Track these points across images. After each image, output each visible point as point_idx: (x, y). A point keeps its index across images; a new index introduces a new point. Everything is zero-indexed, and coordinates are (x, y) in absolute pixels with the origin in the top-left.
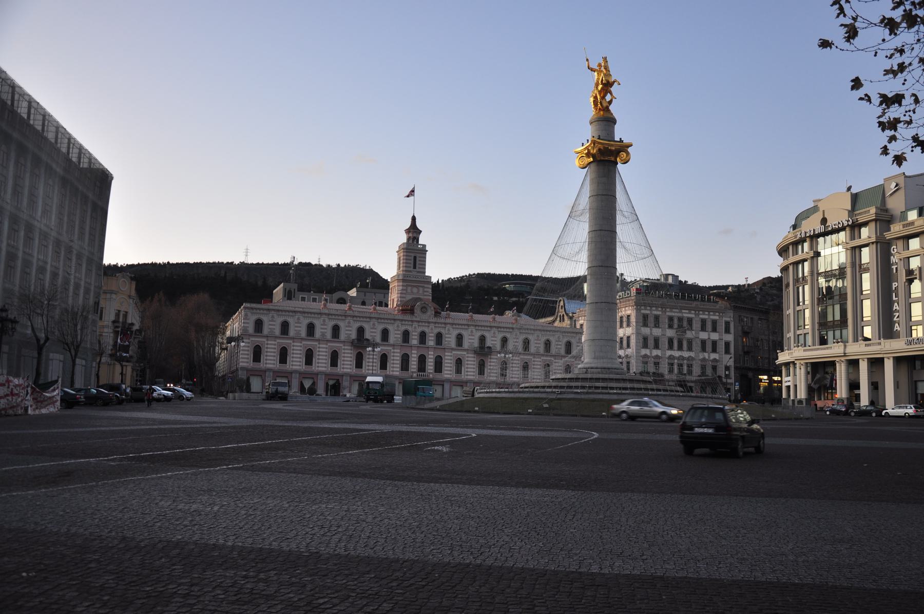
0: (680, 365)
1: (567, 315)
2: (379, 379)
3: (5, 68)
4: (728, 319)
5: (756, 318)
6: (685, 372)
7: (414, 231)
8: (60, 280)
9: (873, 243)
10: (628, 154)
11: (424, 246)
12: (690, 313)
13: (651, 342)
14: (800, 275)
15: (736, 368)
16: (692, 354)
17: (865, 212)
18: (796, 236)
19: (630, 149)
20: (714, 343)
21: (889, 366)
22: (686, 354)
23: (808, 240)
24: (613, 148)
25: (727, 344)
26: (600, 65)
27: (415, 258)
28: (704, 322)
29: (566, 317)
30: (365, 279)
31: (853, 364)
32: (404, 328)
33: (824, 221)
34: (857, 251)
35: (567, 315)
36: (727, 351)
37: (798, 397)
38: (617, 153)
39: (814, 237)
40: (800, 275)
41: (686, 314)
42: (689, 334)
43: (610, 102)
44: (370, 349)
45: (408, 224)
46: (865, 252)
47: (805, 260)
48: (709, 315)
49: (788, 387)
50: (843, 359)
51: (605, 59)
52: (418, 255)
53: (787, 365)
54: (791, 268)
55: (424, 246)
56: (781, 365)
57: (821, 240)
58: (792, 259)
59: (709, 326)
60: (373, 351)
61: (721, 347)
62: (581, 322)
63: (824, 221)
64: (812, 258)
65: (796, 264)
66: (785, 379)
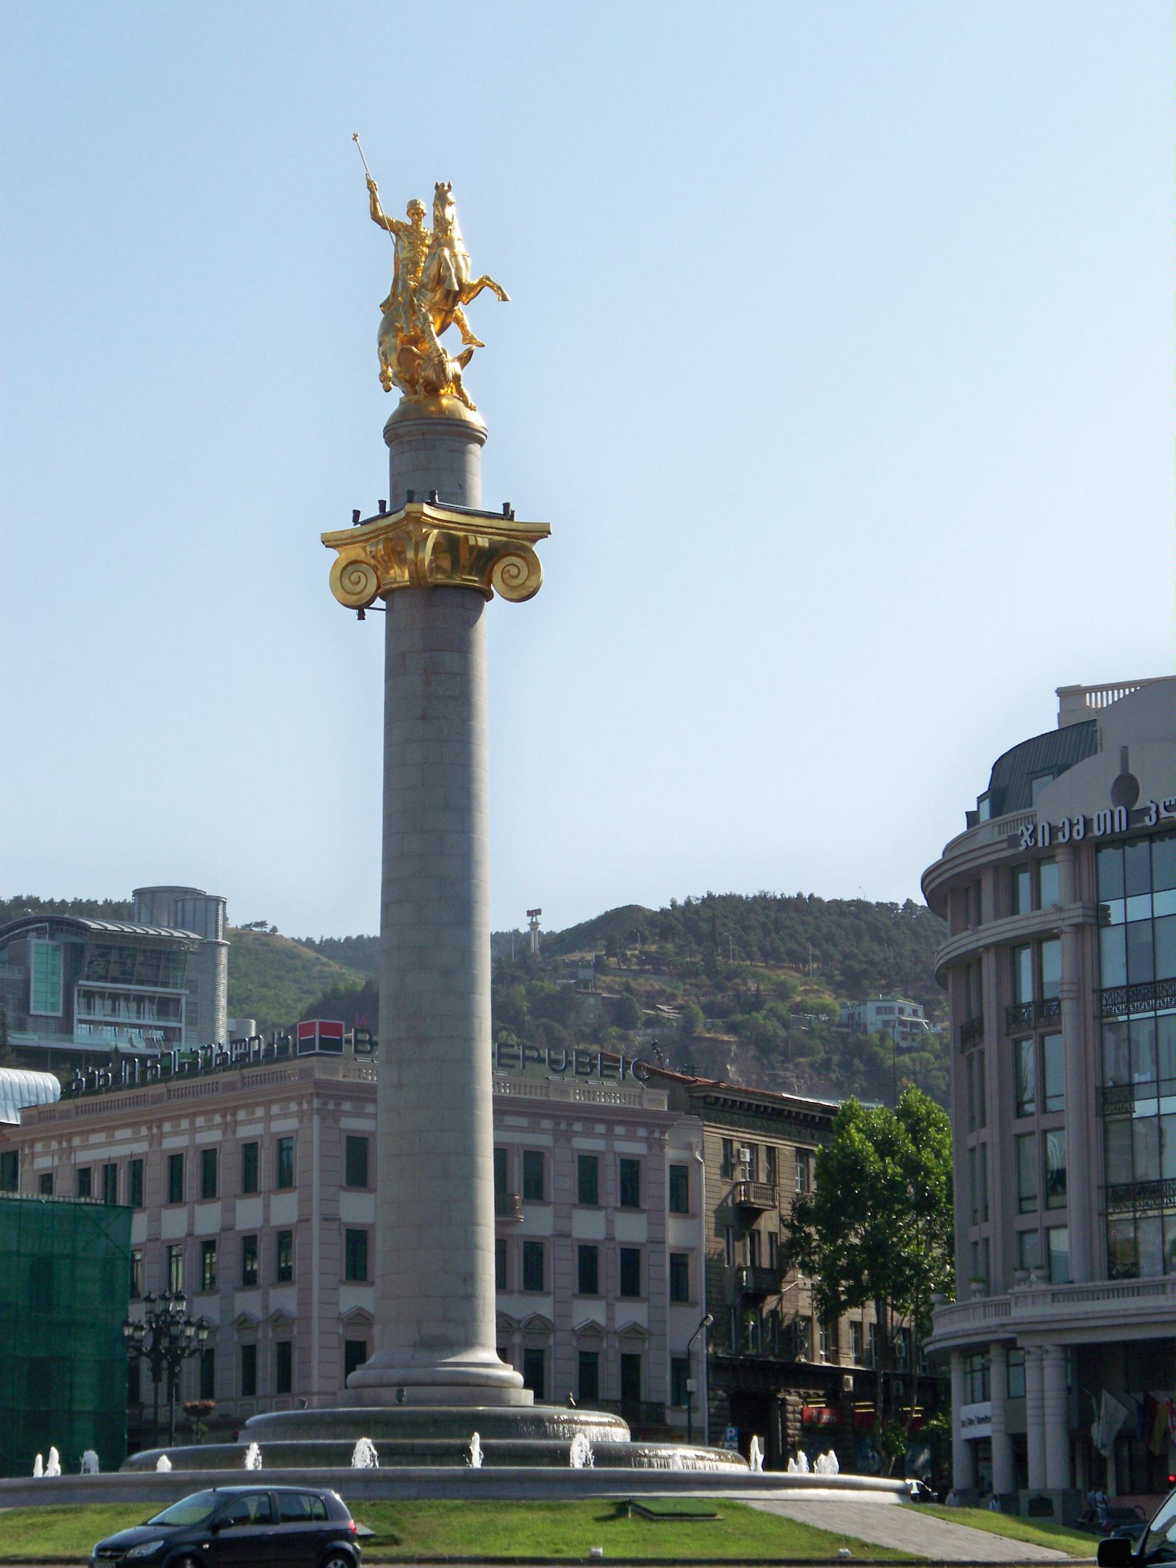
3: (88, 865)
5: (786, 1148)
7: (371, 186)
8: (165, 1375)
10: (533, 565)
12: (534, 1129)
14: (1027, 995)
15: (715, 1365)
18: (1014, 841)
19: (539, 548)
23: (1061, 855)
24: (483, 542)
26: (414, 209)
36: (679, 1292)
38: (485, 560)
39: (1088, 847)
40: (1027, 995)
48: (609, 1136)
49: (979, 1447)
51: (441, 197)
53: (973, 1351)
54: (989, 965)
56: (943, 1356)
57: (1110, 858)
58: (996, 929)
59: (610, 1272)
62: (43, 1163)
63: (1126, 788)
64: (1078, 928)
65: (1010, 948)
66: (962, 1411)
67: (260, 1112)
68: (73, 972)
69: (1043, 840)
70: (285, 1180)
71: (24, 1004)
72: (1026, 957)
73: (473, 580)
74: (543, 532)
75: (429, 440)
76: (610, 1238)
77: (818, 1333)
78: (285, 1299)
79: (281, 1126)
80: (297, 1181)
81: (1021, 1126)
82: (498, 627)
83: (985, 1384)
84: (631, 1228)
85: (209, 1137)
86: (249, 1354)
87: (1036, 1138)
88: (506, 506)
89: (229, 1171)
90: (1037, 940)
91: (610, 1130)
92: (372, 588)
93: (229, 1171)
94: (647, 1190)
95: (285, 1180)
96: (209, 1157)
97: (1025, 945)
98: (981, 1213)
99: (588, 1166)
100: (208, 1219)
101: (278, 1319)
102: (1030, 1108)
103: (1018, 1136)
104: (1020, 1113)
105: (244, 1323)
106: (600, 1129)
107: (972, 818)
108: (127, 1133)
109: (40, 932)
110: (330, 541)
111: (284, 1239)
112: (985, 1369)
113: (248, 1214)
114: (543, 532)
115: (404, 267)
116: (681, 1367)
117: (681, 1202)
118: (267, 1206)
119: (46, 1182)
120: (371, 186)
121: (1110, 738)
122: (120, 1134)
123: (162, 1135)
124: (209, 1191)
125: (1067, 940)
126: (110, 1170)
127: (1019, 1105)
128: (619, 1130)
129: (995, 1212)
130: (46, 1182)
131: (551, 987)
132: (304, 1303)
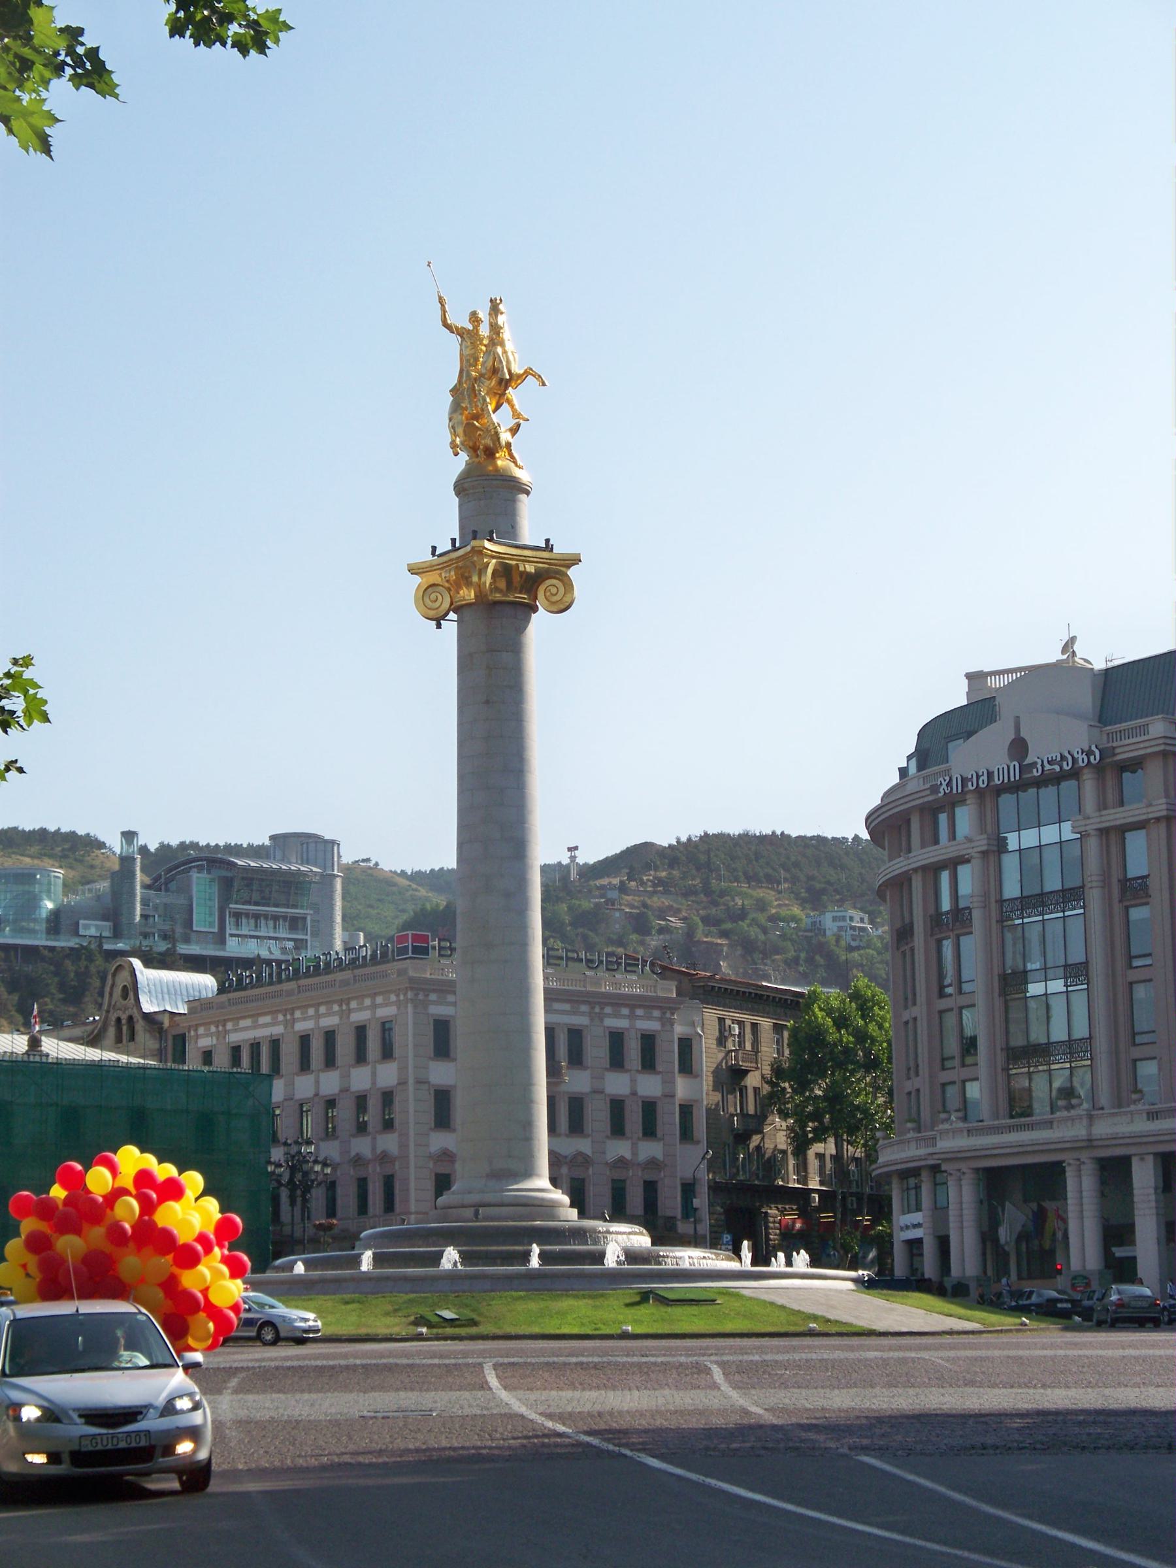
9: (1158, 819)
10: (568, 585)
13: (634, 1119)
14: (946, 905)
15: (715, 1188)
17: (1131, 732)
18: (935, 789)
19: (572, 572)
21: (1144, 1177)
23: (971, 799)
24: (530, 568)
26: (474, 318)
28: (617, 1040)
29: (140, 1025)
31: (1114, 1172)
33: (1019, 747)
34: (1113, 837)
36: (686, 1133)
37: (955, 1271)
38: (532, 583)
39: (990, 793)
40: (946, 905)
46: (1136, 843)
47: (964, 860)
48: (632, 1017)
49: (914, 1245)
50: (1084, 1156)
53: (909, 1174)
54: (917, 882)
58: (922, 856)
59: (634, 1119)
61: (670, 1120)
62: (205, 1043)
63: (1019, 747)
64: (985, 854)
65: (933, 871)
67: (368, 1002)
69: (956, 788)
70: (387, 1053)
71: (189, 923)
72: (945, 876)
73: (524, 597)
74: (575, 560)
75: (488, 491)
76: (634, 1093)
78: (389, 1142)
80: (397, 1052)
81: (944, 1004)
82: (541, 627)
84: (617, 1084)
86: (362, 1183)
87: (956, 1011)
89: (345, 1047)
90: (953, 864)
92: (446, 605)
93: (345, 1047)
95: (387, 1053)
100: (330, 1083)
101: (384, 1158)
104: (942, 995)
105: (358, 1161)
106: (625, 1011)
107: (903, 772)
108: (267, 1019)
109: (200, 869)
110: (414, 570)
111: (387, 1097)
112: (918, 1188)
113: (360, 1079)
114: (575, 560)
115: (467, 361)
116: (688, 1189)
117: (687, 1065)
119: (207, 1057)
121: (1007, 710)
123: (294, 1020)
124: (330, 1061)
125: (976, 863)
126: (255, 1047)
127: (941, 988)
128: (640, 1012)
129: (924, 1070)
130: (207, 1057)
131: (586, 904)
132: (403, 1146)
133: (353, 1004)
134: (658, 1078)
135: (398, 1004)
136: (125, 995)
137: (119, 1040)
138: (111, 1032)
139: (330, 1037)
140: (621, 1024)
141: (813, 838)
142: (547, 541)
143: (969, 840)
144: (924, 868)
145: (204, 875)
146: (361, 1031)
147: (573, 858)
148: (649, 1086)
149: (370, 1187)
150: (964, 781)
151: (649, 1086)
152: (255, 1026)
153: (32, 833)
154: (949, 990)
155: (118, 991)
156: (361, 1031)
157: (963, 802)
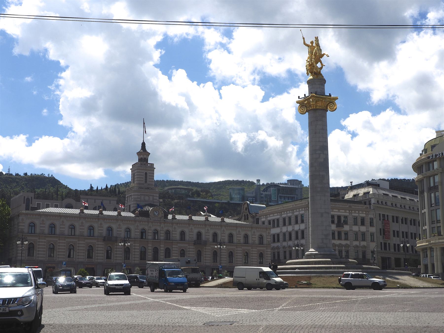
0: (340, 252)
1: (250, 214)
2: (388, 278)
4: (372, 216)
6: (344, 256)
7: (304, 38)
11: (152, 165)
14: (432, 185)
16: (348, 242)
19: (336, 101)
20: (363, 234)
22: (344, 242)
25: (372, 235)
27: (146, 173)
28: (355, 219)
29: (249, 216)
30: (253, 183)
32: (141, 227)
35: (250, 214)
40: (432, 185)
41: (342, 213)
42: (346, 228)
43: (321, 68)
44: (18, 243)
45: (139, 148)
48: (359, 213)
52: (148, 172)
55: (152, 165)
60: (22, 243)
61: (368, 237)
62: (263, 219)
67: (298, 210)
68: (278, 193)
69: (434, 157)
70: (302, 221)
71: (271, 198)
72: (432, 178)
74: (170, 78)
76: (360, 231)
77: (227, 279)
79: (301, 212)
80: (305, 221)
81: (432, 208)
83: (427, 255)
85: (290, 215)
86: (285, 252)
87: (435, 211)
88: (330, 94)
89: (293, 220)
90: (434, 176)
91: (359, 212)
92: (305, 111)
93: (293, 220)
94: (365, 222)
95: (302, 221)
96: (290, 218)
97: (431, 176)
98: (424, 224)
99: (355, 219)
100: (290, 228)
102: (433, 205)
103: (431, 210)
104: (431, 206)
105: (284, 247)
106: (357, 212)
107: (421, 154)
108: (276, 214)
111: (303, 232)
112: (427, 252)
113: (297, 227)
114: (170, 78)
115: (311, 53)
117: (371, 224)
118: (300, 226)
119: (263, 223)
120: (304, 38)
122: (275, 215)
123: (282, 215)
124: (290, 224)
125: (439, 175)
126: (274, 221)
127: (431, 205)
128: (360, 212)
130: (263, 223)
133: (295, 211)
134: (365, 227)
135: (305, 210)
136: (246, 210)
137: (245, 219)
138: (243, 218)
139: (290, 218)
140: (357, 215)
141: (403, 179)
142: (330, 94)
143: (437, 169)
144: (427, 177)
145: (274, 188)
146: (296, 217)
147: (351, 184)
148: (363, 229)
149: (280, 254)
150: (436, 155)
151: (363, 229)
152: (274, 216)
153: (241, 181)
154: (433, 205)
155: (245, 209)
156: (296, 217)
157: (436, 161)
